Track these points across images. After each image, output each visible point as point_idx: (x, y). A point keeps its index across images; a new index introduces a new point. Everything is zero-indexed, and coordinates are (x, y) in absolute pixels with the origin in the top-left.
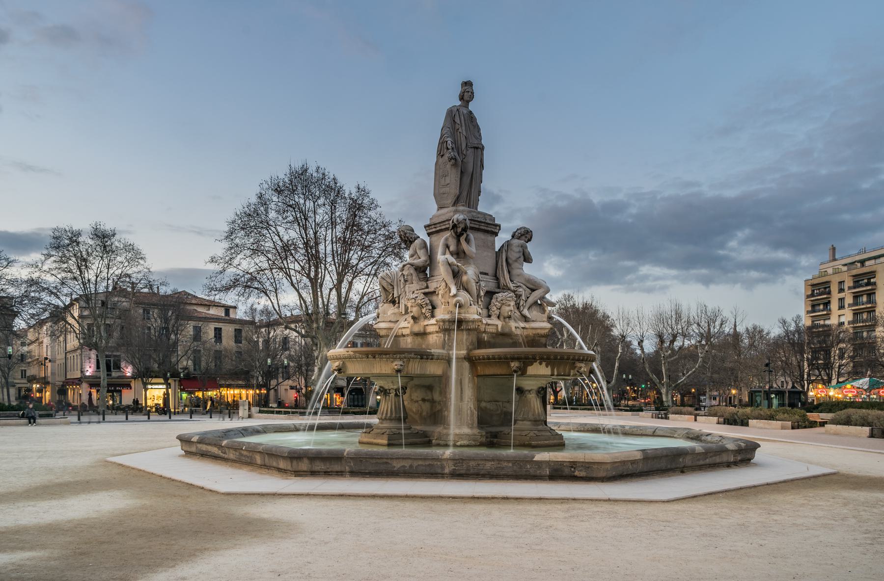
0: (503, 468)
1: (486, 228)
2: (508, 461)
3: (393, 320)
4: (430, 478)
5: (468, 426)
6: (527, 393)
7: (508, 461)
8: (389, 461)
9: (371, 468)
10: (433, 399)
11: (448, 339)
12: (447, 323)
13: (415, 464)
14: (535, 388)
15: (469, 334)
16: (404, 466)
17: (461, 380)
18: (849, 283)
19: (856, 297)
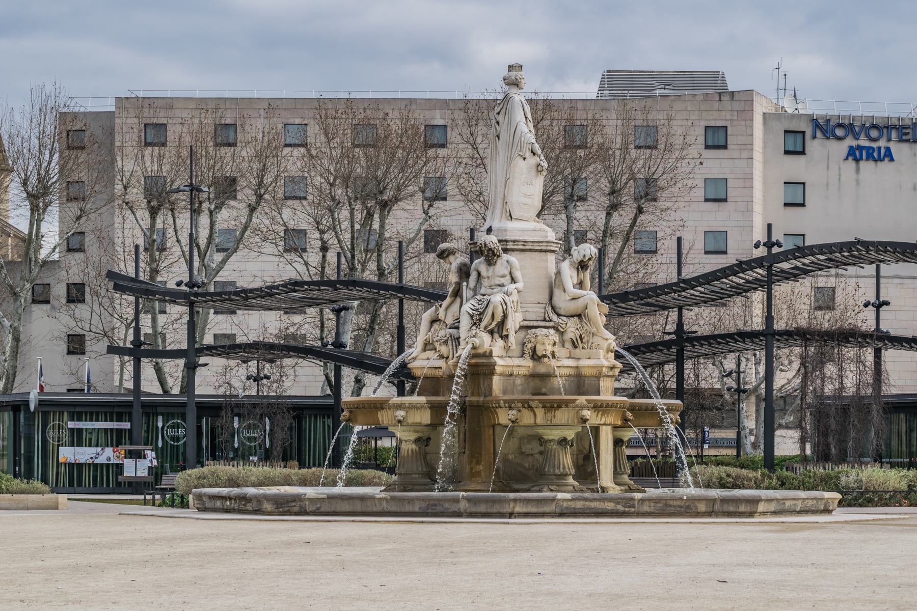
1: (532, 248)
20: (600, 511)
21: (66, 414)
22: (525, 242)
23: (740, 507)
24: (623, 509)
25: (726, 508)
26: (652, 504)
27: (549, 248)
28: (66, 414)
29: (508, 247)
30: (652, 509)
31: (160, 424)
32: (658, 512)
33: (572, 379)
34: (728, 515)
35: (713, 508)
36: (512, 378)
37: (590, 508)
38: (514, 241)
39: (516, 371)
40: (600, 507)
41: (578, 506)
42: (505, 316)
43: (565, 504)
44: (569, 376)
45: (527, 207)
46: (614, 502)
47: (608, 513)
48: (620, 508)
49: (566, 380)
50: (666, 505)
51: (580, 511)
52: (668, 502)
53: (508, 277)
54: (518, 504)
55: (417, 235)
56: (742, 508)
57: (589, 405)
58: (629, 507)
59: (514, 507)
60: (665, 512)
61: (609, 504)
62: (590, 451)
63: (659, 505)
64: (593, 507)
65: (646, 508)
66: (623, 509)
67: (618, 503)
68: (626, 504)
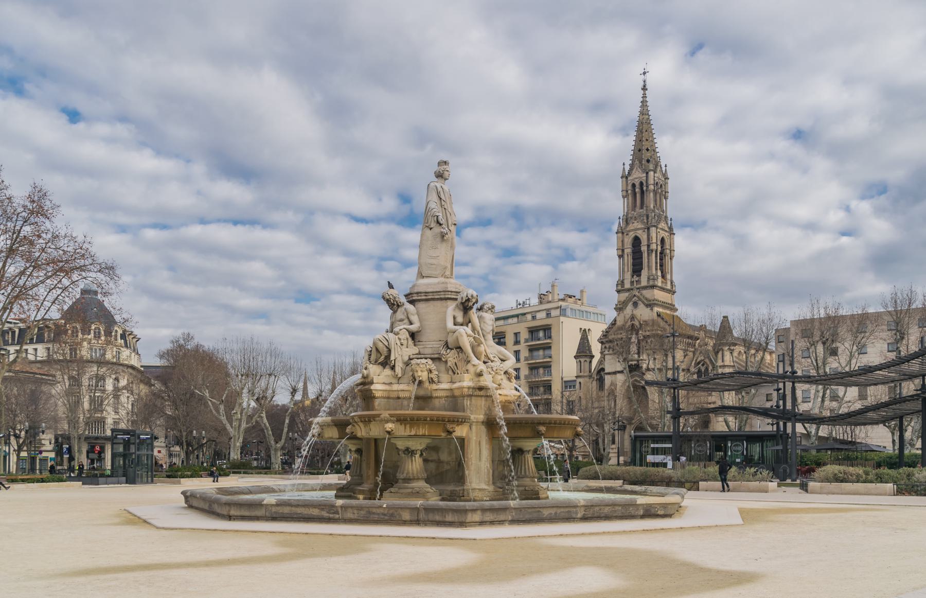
0: (615, 511)
1: (433, 297)
2: (620, 505)
3: (386, 382)
4: (565, 522)
5: (485, 483)
6: (525, 453)
7: (620, 505)
8: (541, 510)
9: (527, 517)
10: (439, 460)
11: (470, 404)
12: (471, 390)
13: (559, 511)
14: (532, 449)
15: (486, 400)
16: (551, 514)
17: (480, 442)
18: (524, 335)
19: (532, 349)
20: (306, 516)
21: (650, 441)
22: (426, 293)
23: (447, 516)
24: (327, 515)
25: (431, 517)
26: (356, 512)
27: (447, 296)
28: (650, 441)
29: (414, 298)
30: (356, 516)
31: (729, 445)
32: (362, 519)
33: (451, 399)
34: (438, 524)
35: (418, 516)
36: (400, 400)
37: (296, 514)
38: (417, 293)
39: (402, 395)
40: (306, 512)
41: (286, 512)
42: (390, 351)
43: (274, 509)
44: (447, 397)
45: (433, 266)
46: (319, 509)
47: (314, 519)
48: (325, 514)
49: (445, 401)
50: (369, 512)
51: (288, 515)
52: (371, 509)
53: (406, 321)
54: (233, 508)
55: (10, 266)
56: (449, 518)
57: (392, 418)
58: (334, 513)
59: (229, 511)
60: (369, 519)
61: (314, 510)
62: (461, 459)
63: (362, 512)
64: (299, 512)
65: (349, 515)
66: (327, 515)
67: (323, 509)
68: (329, 510)
